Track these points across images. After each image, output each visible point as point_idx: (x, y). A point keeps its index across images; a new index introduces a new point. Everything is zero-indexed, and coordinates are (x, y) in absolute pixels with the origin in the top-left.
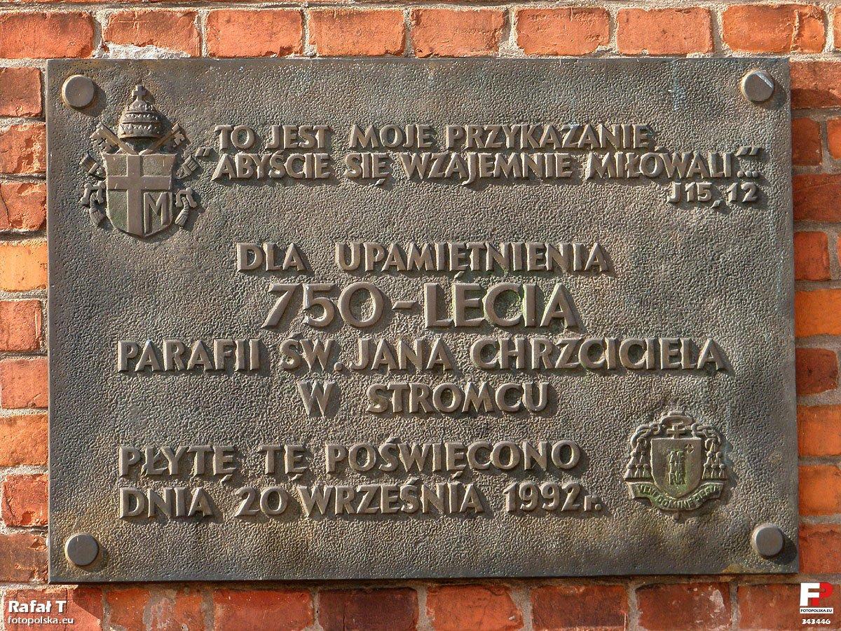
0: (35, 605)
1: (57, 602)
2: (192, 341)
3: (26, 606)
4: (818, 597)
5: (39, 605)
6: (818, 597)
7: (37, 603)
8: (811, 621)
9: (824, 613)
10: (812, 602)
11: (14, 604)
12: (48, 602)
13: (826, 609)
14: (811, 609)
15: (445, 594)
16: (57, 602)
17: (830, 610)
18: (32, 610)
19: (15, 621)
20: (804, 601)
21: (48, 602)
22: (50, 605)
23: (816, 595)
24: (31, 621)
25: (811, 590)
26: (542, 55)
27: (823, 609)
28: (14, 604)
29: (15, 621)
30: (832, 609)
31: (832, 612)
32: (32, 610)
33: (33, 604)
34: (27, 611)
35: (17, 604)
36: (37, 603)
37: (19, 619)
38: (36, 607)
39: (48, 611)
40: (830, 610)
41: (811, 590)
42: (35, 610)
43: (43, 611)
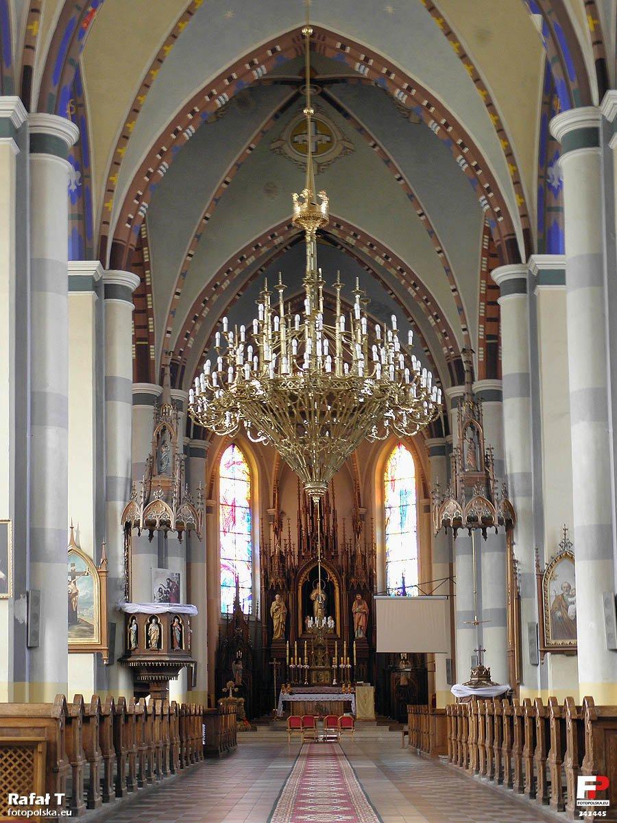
0: (34, 797)
1: (56, 795)
2: (263, 434)
3: (25, 799)
4: (595, 789)
5: (38, 797)
6: (595, 789)
7: (36, 796)
8: (152, 678)
9: (601, 805)
10: (589, 795)
11: (14, 797)
12: (47, 795)
13: (602, 801)
14: (588, 801)
15: (558, 656)
16: (56, 795)
17: (607, 803)
18: (31, 803)
19: (14, 813)
20: (581, 795)
21: (47, 795)
22: (49, 798)
23: (593, 788)
24: (30, 813)
25: (588, 783)
26: (80, 775)
27: (600, 801)
28: (14, 797)
29: (14, 813)
30: (608, 801)
31: (608, 805)
32: (31, 803)
33: (32, 796)
34: (26, 803)
35: (17, 796)
36: (36, 796)
37: (19, 811)
38: (35, 800)
39: (47, 803)
40: (607, 803)
41: (588, 783)
42: (34, 802)
43: (42, 803)
